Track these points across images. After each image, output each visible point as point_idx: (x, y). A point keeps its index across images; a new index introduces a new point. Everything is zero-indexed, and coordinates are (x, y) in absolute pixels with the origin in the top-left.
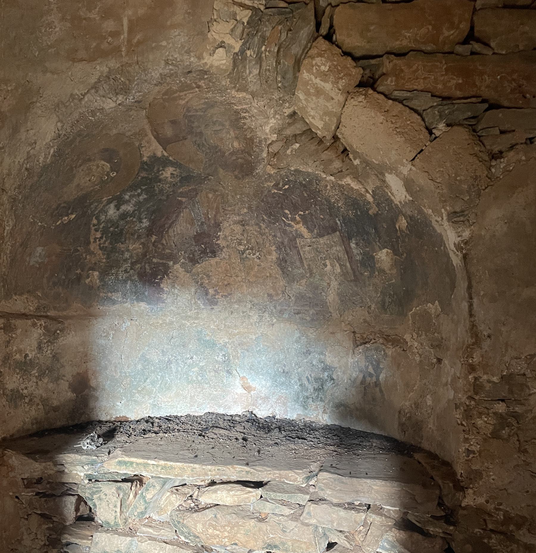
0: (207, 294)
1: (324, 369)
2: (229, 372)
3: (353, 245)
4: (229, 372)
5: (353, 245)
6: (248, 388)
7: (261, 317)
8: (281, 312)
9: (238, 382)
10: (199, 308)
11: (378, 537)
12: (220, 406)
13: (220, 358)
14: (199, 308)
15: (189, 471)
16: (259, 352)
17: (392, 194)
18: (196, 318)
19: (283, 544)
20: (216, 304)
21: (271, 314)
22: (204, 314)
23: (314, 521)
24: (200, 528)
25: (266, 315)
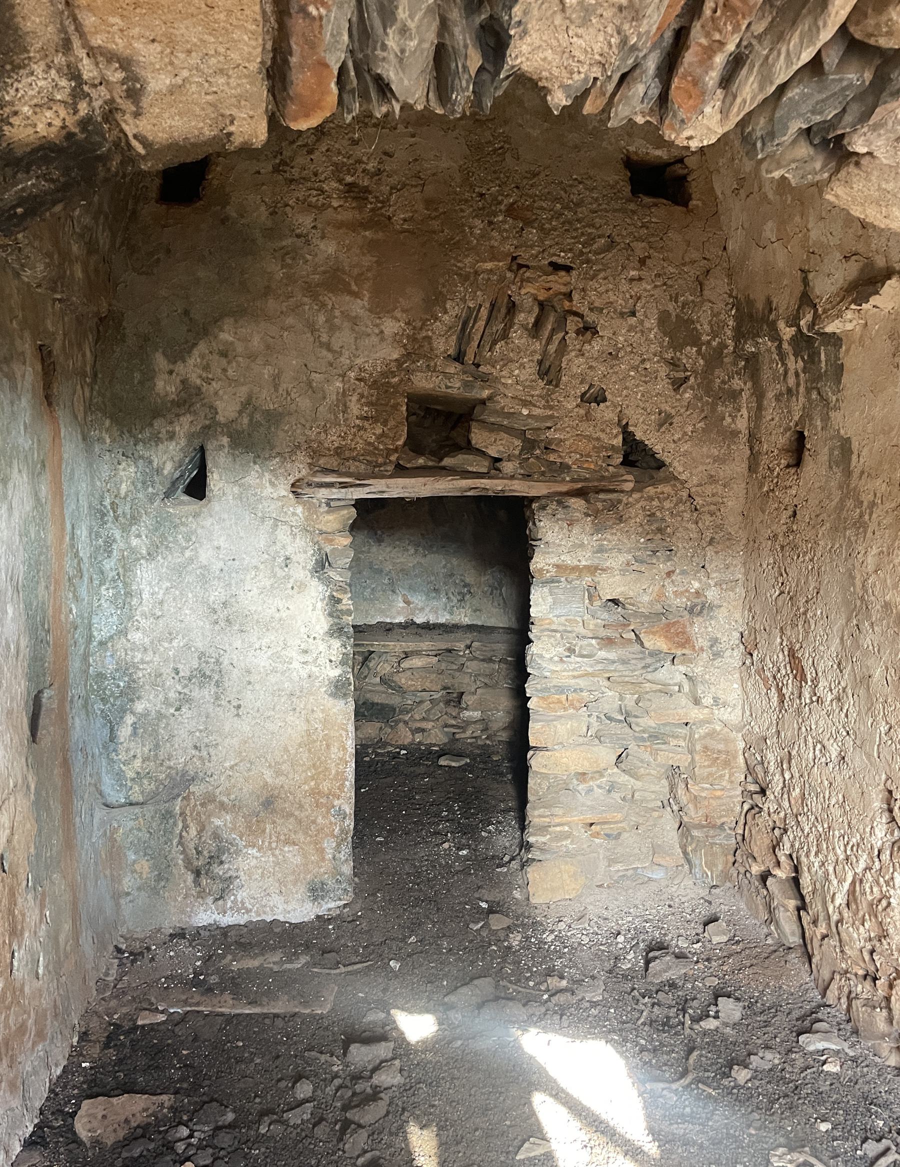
0: (376, 534)
1: (465, 586)
2: (394, 591)
3: (482, 505)
4: (394, 591)
5: (482, 505)
6: (408, 602)
7: (416, 551)
8: (431, 546)
9: (400, 599)
10: (370, 545)
11: (609, 185)
12: (387, 617)
13: (386, 581)
14: (370, 545)
15: (398, 647)
16: (416, 576)
17: (427, 65)
18: (369, 552)
19: (453, 686)
20: (383, 541)
21: (424, 548)
22: (374, 549)
23: (470, 671)
24: (403, 681)
25: (420, 549)
